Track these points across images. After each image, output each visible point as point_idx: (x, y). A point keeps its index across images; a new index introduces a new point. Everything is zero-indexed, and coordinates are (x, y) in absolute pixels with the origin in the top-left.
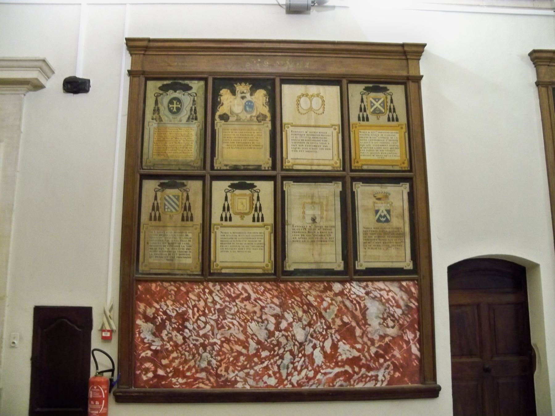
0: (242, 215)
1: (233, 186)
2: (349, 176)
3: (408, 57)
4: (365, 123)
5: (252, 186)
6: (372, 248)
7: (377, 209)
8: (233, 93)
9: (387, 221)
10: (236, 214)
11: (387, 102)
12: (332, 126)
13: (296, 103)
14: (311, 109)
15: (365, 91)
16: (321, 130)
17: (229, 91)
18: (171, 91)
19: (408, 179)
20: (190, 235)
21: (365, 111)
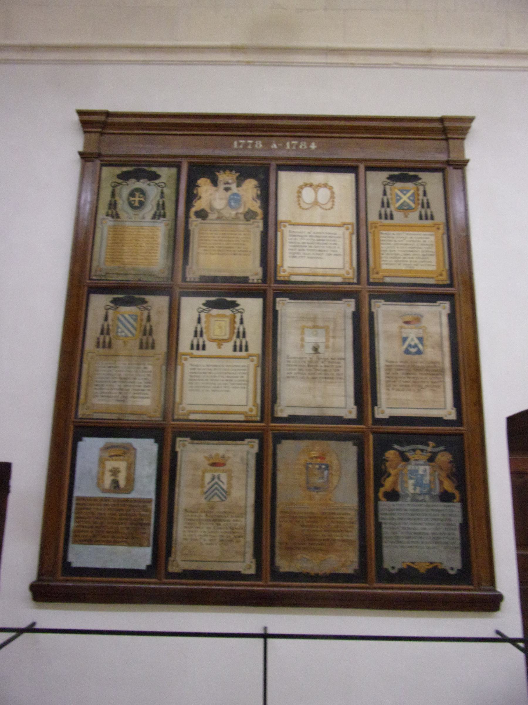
0: (220, 342)
1: (209, 304)
2: (363, 292)
3: (449, 136)
4: (388, 222)
5: (234, 305)
6: (398, 390)
7: (404, 335)
8: (215, 182)
9: (419, 352)
10: (212, 340)
11: (418, 195)
12: (344, 224)
13: (297, 194)
14: (316, 203)
15: (389, 181)
16: (328, 230)
17: (209, 181)
18: (133, 180)
19: (449, 297)
20: (150, 368)
21: (388, 206)
